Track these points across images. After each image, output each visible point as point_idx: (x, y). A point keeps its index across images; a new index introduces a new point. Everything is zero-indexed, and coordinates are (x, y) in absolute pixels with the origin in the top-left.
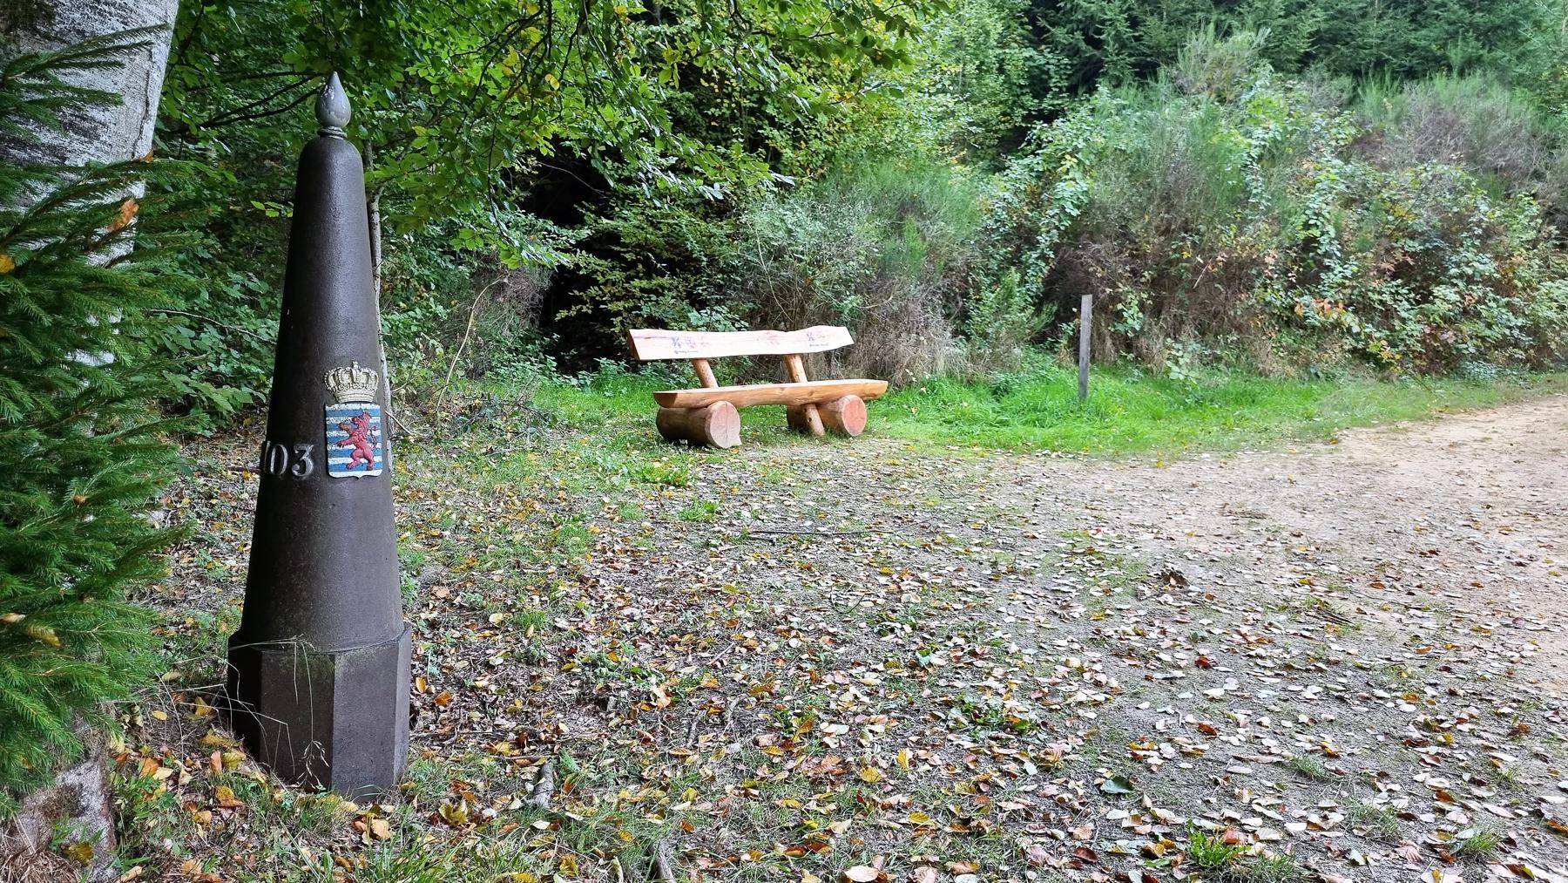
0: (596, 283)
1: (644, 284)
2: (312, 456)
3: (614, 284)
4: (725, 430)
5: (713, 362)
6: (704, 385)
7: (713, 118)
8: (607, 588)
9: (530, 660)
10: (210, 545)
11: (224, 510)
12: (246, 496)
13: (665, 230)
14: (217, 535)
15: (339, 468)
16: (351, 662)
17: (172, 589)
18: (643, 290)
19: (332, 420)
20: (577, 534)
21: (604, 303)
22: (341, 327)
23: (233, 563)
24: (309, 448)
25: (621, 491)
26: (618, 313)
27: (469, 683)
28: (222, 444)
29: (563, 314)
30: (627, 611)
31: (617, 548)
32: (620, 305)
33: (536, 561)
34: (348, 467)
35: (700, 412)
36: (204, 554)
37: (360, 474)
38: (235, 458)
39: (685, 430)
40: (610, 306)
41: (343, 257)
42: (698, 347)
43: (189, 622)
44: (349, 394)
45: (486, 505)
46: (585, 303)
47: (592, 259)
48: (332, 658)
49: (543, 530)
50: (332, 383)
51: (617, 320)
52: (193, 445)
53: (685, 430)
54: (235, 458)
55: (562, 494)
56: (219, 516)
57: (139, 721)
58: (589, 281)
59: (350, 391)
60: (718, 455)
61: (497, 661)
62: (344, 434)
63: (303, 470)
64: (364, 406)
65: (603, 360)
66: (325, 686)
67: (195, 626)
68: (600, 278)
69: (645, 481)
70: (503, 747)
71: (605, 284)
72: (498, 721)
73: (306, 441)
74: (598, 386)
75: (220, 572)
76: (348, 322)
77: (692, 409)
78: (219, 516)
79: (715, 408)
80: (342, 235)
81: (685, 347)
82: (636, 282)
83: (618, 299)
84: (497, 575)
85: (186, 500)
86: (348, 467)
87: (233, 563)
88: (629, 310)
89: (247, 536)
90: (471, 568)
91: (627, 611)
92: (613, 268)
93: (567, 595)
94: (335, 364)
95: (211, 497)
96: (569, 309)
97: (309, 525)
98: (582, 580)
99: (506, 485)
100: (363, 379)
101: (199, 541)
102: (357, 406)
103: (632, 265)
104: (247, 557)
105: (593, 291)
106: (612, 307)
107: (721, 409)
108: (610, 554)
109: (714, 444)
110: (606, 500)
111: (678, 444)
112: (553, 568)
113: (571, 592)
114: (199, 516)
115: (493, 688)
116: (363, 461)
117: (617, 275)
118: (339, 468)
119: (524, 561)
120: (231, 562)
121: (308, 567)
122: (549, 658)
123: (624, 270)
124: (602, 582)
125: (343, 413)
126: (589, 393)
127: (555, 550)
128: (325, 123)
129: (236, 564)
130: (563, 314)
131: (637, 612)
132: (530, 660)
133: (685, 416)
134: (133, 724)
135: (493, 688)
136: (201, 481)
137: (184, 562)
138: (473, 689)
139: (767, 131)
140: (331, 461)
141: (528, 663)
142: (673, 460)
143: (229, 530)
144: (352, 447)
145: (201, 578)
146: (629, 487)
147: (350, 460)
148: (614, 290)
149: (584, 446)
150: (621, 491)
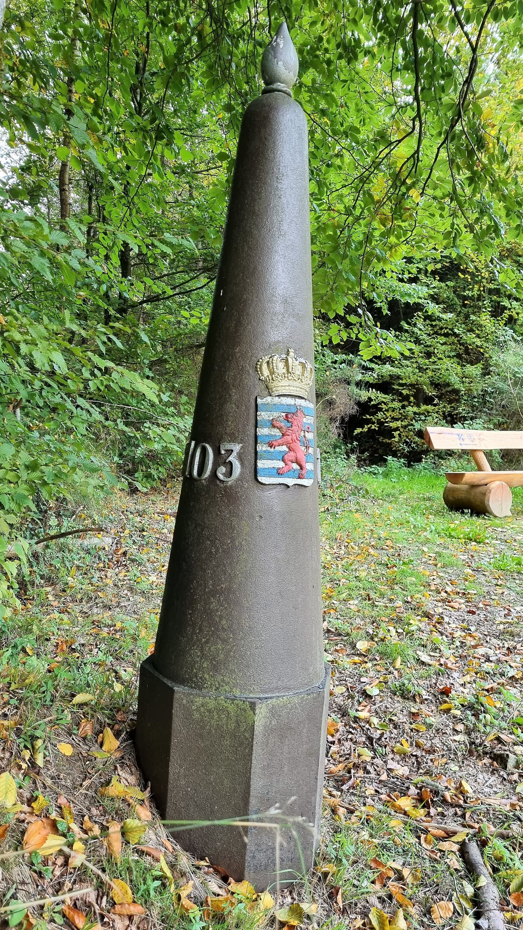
0: (381, 410)
1: (415, 409)
2: (241, 457)
3: (394, 410)
4: (500, 502)
5: (489, 454)
6: (480, 469)
7: (465, 298)
8: (452, 625)
9: (405, 695)
10: (140, 564)
11: (151, 540)
12: (165, 531)
13: (430, 374)
14: (145, 557)
15: (269, 473)
16: (273, 712)
17: (110, 597)
18: (415, 413)
19: (263, 416)
20: (412, 575)
21: (387, 422)
22: (278, 307)
23: (154, 579)
24: (237, 448)
25: (434, 543)
26: (397, 429)
27: (352, 713)
28: (152, 497)
29: (358, 430)
30: (481, 651)
31: (448, 589)
32: (399, 424)
33: (382, 596)
34: (279, 473)
35: (481, 489)
36: (134, 570)
37: (291, 482)
38: (160, 506)
39: (468, 503)
40: (391, 425)
41: (285, 227)
42: (477, 442)
43: (119, 625)
44: (282, 385)
45: (331, 548)
46: (373, 423)
47: (380, 395)
48: (253, 706)
49: (381, 570)
50: (266, 372)
51: (396, 434)
52: (135, 496)
53: (468, 503)
54: (160, 506)
55: (389, 542)
56: (147, 544)
57: (40, 762)
58: (377, 408)
59: (285, 382)
60: (497, 522)
61: (374, 691)
62: (276, 432)
63: (230, 473)
64: (299, 402)
65: (390, 458)
66: (243, 742)
67: (122, 630)
68: (384, 406)
69: (451, 536)
70: (406, 803)
71: (387, 410)
72: (392, 765)
73: (233, 439)
74: (386, 475)
75: (144, 586)
76: (285, 302)
77: (473, 486)
78: (147, 544)
79: (493, 486)
80: (284, 200)
81: (467, 441)
82: (409, 408)
83: (397, 420)
84: (354, 604)
85: (127, 531)
86: (279, 473)
87: (154, 579)
88: (405, 427)
89: (165, 559)
90: (330, 597)
91: (481, 651)
92: (394, 400)
93: (420, 630)
94: (271, 349)
95: (143, 530)
96: (363, 427)
97: (233, 540)
98: (427, 615)
99: (344, 535)
100: (298, 370)
101: (133, 561)
102: (290, 401)
103: (406, 398)
104: (164, 575)
105: (380, 415)
106: (393, 425)
107: (498, 486)
108: (444, 594)
109: (491, 513)
110: (426, 549)
111: (463, 513)
112: (399, 603)
113: (422, 626)
114: (134, 542)
115: (375, 721)
116: (295, 466)
117: (396, 405)
118: (269, 473)
119: (372, 596)
120: (153, 578)
121: (229, 589)
122: (425, 695)
123: (400, 401)
124: (446, 619)
125: (275, 407)
126: (381, 479)
127: (396, 587)
128: (270, 78)
129: (156, 580)
130: (358, 430)
131: (491, 652)
132: (405, 695)
133: (468, 491)
134: (33, 764)
135: (375, 721)
136: (138, 519)
137: (121, 576)
138: (356, 719)
139: (506, 303)
140: (261, 464)
141: (403, 696)
142: (463, 523)
143: (153, 554)
144: (284, 448)
145: (131, 589)
146: (439, 541)
147: (281, 464)
148: (393, 414)
149: (393, 512)
150: (434, 543)
